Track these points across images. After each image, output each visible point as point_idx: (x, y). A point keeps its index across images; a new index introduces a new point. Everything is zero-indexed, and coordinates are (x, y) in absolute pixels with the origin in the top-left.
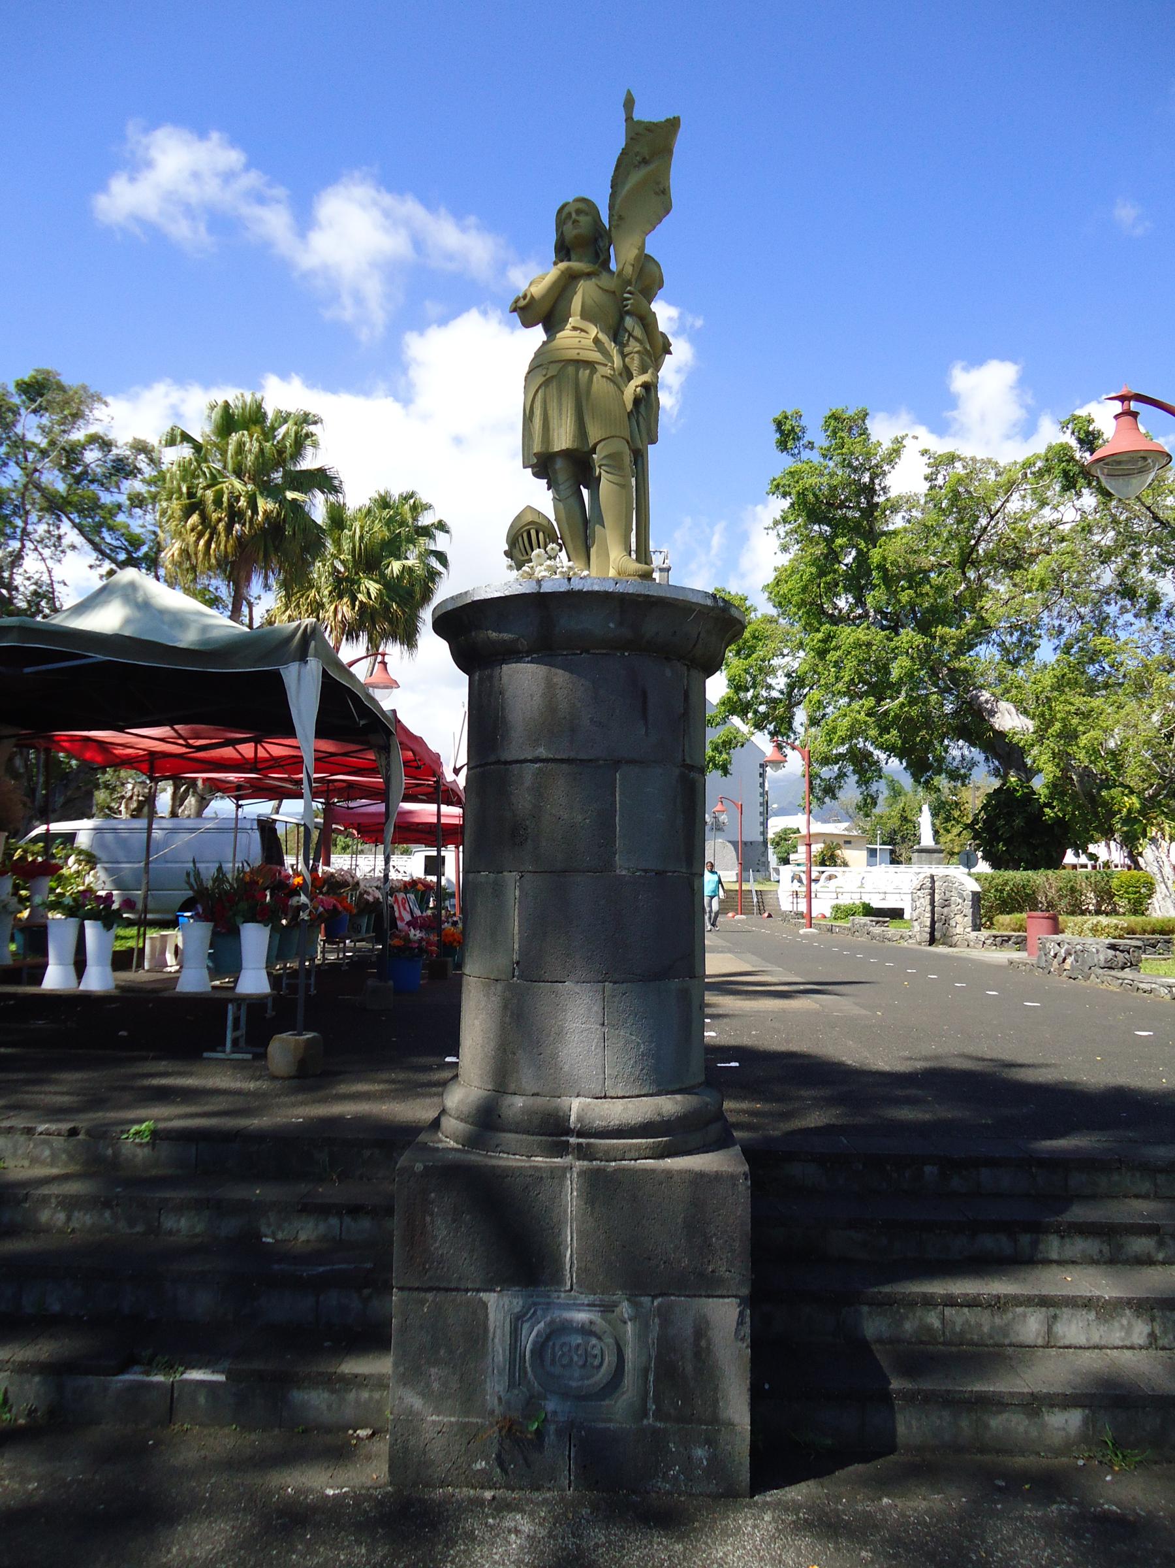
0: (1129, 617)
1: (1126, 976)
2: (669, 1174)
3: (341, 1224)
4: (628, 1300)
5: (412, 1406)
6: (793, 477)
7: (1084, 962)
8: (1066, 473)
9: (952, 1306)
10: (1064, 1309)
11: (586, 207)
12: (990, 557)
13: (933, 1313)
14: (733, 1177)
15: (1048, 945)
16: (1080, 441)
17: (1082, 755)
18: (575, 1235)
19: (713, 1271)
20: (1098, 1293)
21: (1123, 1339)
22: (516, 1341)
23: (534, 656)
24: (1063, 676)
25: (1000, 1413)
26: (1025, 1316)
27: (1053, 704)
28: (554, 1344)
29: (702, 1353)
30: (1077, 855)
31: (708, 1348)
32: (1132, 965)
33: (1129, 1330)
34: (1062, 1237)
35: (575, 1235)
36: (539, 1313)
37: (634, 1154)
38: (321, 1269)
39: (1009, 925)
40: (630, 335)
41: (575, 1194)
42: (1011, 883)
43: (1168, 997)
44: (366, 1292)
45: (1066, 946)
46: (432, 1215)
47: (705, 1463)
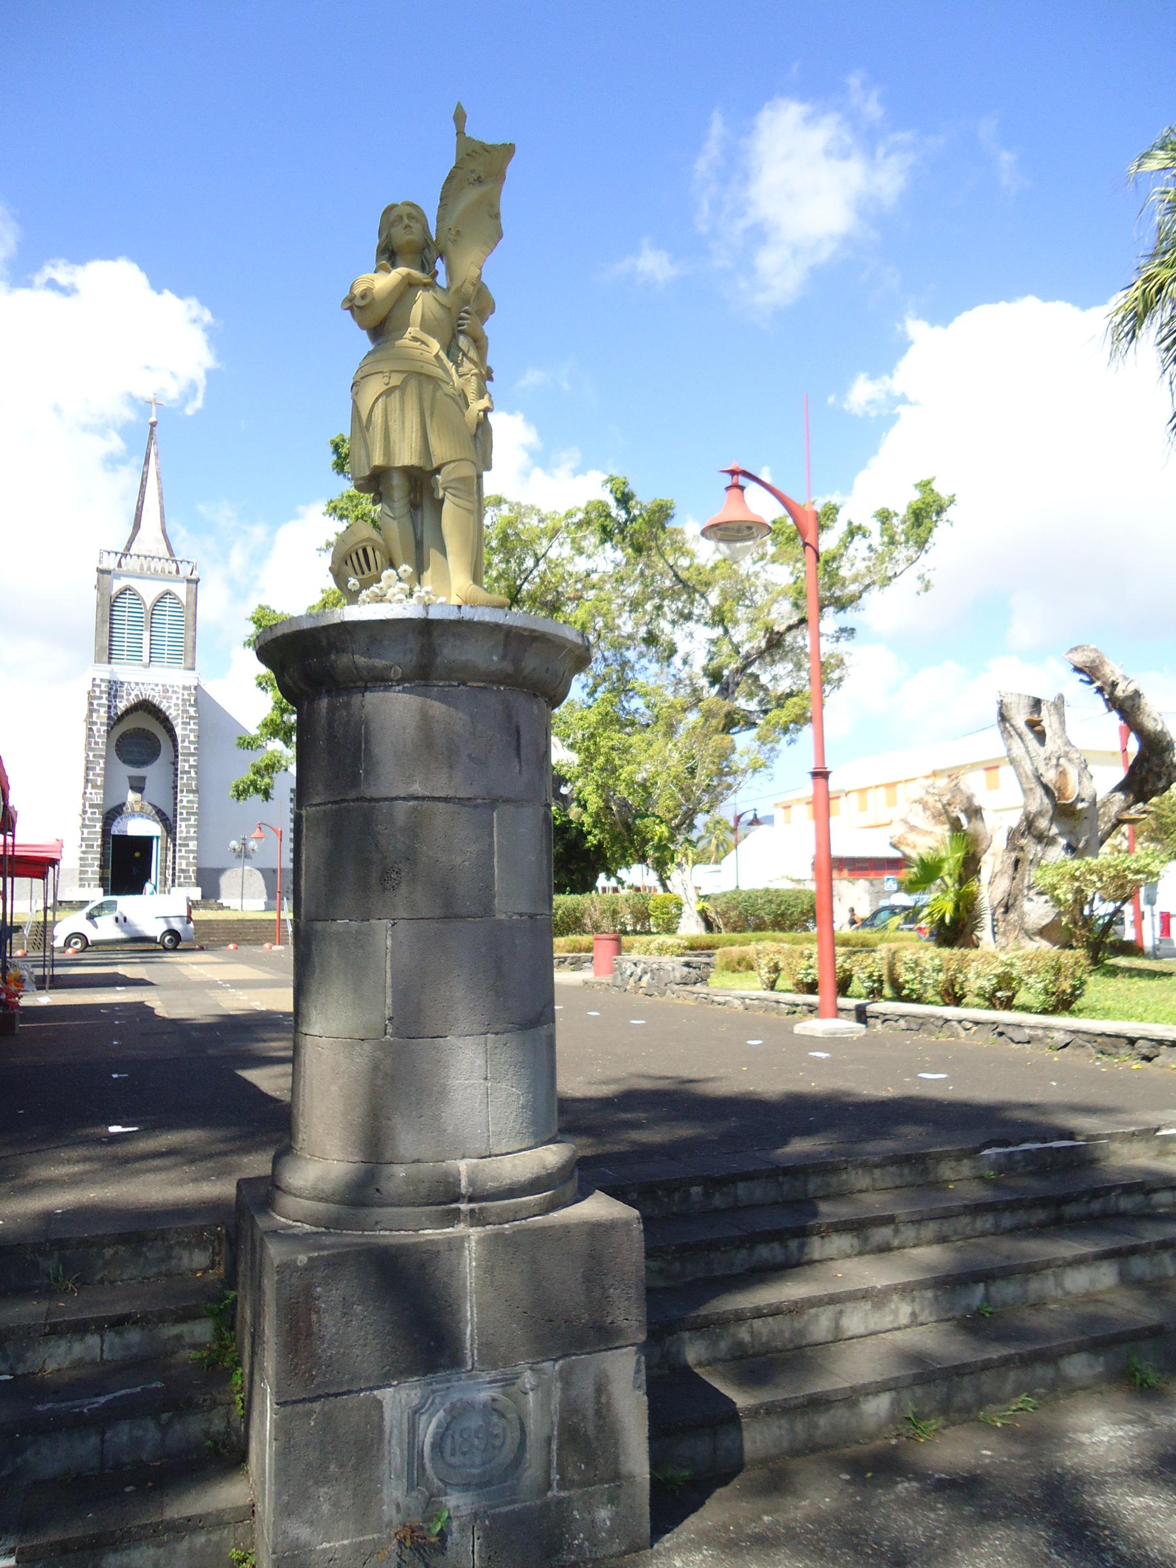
0: (644, 661)
1: (700, 991)
2: (566, 1229)
3: (103, 1342)
4: (530, 1369)
5: (298, 1539)
6: (352, 501)
7: (660, 979)
8: (604, 528)
9: (759, 1317)
10: (848, 1304)
11: (415, 214)
12: (532, 597)
13: (743, 1328)
14: (627, 1223)
15: (624, 965)
16: (618, 500)
17: (622, 787)
18: (475, 1309)
19: (612, 1323)
20: (872, 1285)
21: (892, 1322)
22: (414, 1438)
23: (406, 685)
24: (607, 714)
25: (828, 1410)
26: (817, 1316)
27: (598, 739)
28: (454, 1432)
29: (603, 1411)
30: (608, 879)
31: (608, 1403)
32: (703, 980)
33: (896, 1313)
34: (823, 1237)
35: (475, 1309)
36: (438, 1400)
37: (524, 1214)
38: (102, 1400)
39: (564, 947)
40: (464, 355)
41: (474, 1264)
42: (563, 907)
43: (741, 1008)
44: (165, 1416)
45: (642, 965)
46: (317, 1312)
47: (608, 1523)
